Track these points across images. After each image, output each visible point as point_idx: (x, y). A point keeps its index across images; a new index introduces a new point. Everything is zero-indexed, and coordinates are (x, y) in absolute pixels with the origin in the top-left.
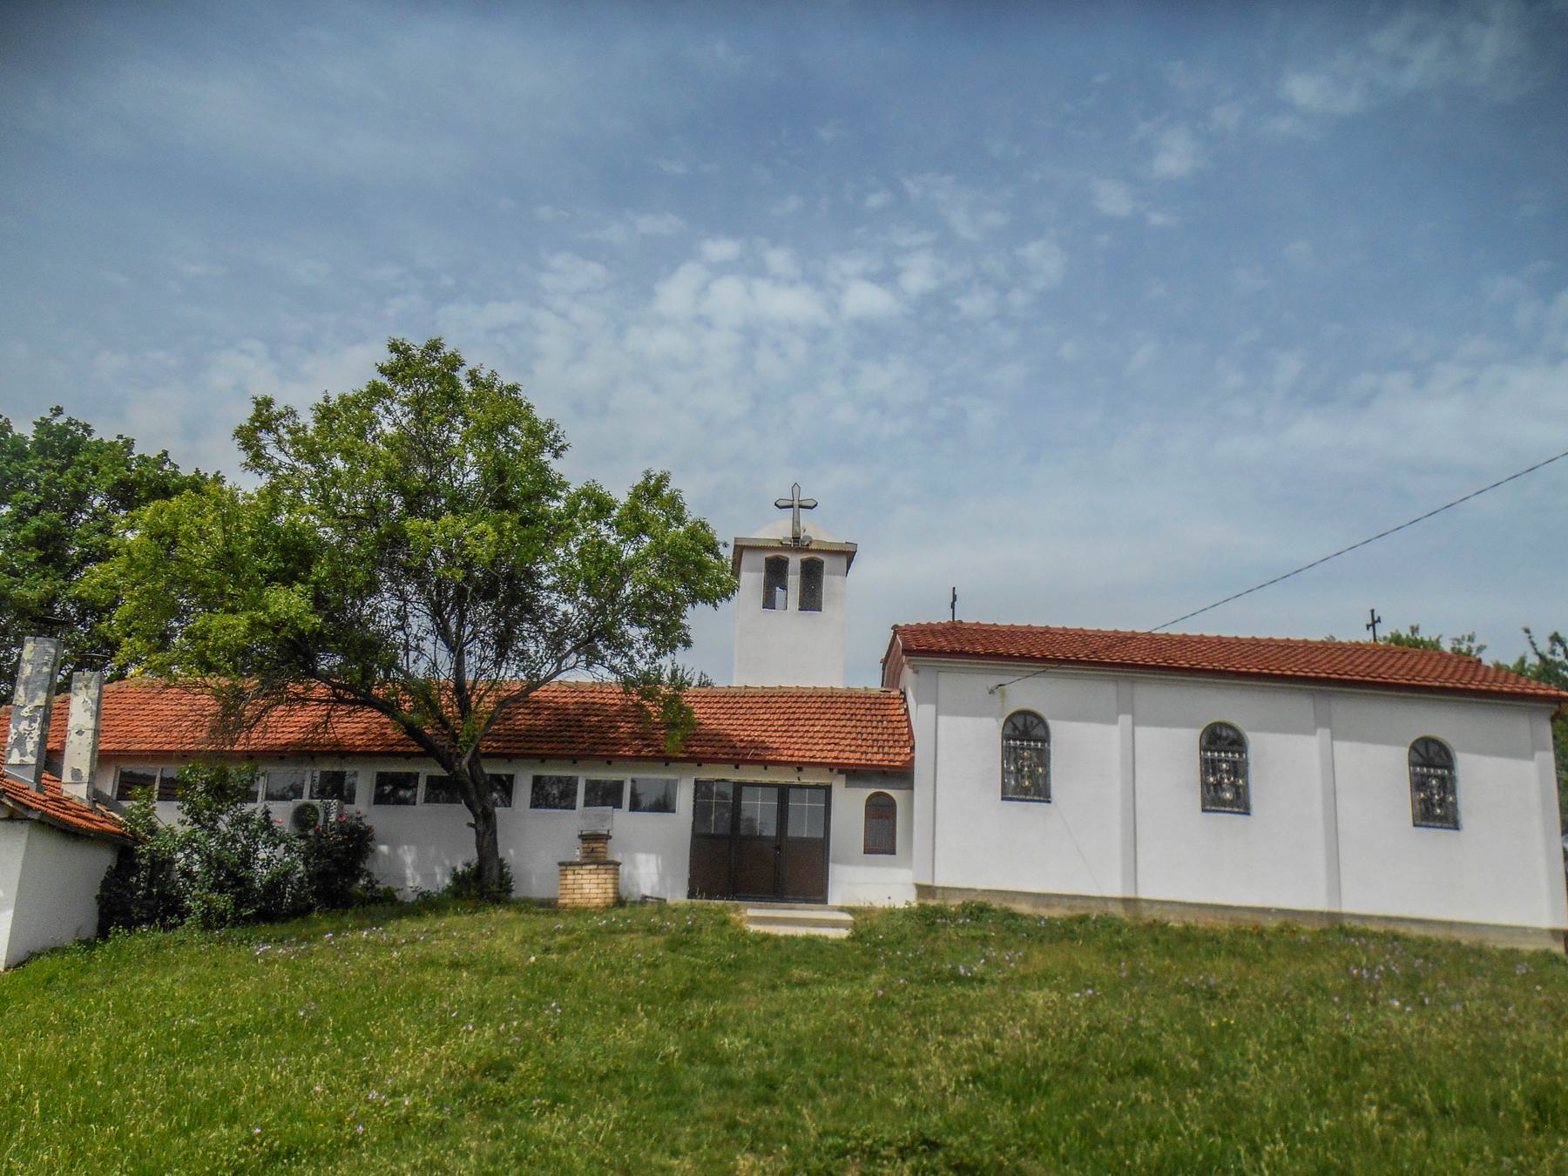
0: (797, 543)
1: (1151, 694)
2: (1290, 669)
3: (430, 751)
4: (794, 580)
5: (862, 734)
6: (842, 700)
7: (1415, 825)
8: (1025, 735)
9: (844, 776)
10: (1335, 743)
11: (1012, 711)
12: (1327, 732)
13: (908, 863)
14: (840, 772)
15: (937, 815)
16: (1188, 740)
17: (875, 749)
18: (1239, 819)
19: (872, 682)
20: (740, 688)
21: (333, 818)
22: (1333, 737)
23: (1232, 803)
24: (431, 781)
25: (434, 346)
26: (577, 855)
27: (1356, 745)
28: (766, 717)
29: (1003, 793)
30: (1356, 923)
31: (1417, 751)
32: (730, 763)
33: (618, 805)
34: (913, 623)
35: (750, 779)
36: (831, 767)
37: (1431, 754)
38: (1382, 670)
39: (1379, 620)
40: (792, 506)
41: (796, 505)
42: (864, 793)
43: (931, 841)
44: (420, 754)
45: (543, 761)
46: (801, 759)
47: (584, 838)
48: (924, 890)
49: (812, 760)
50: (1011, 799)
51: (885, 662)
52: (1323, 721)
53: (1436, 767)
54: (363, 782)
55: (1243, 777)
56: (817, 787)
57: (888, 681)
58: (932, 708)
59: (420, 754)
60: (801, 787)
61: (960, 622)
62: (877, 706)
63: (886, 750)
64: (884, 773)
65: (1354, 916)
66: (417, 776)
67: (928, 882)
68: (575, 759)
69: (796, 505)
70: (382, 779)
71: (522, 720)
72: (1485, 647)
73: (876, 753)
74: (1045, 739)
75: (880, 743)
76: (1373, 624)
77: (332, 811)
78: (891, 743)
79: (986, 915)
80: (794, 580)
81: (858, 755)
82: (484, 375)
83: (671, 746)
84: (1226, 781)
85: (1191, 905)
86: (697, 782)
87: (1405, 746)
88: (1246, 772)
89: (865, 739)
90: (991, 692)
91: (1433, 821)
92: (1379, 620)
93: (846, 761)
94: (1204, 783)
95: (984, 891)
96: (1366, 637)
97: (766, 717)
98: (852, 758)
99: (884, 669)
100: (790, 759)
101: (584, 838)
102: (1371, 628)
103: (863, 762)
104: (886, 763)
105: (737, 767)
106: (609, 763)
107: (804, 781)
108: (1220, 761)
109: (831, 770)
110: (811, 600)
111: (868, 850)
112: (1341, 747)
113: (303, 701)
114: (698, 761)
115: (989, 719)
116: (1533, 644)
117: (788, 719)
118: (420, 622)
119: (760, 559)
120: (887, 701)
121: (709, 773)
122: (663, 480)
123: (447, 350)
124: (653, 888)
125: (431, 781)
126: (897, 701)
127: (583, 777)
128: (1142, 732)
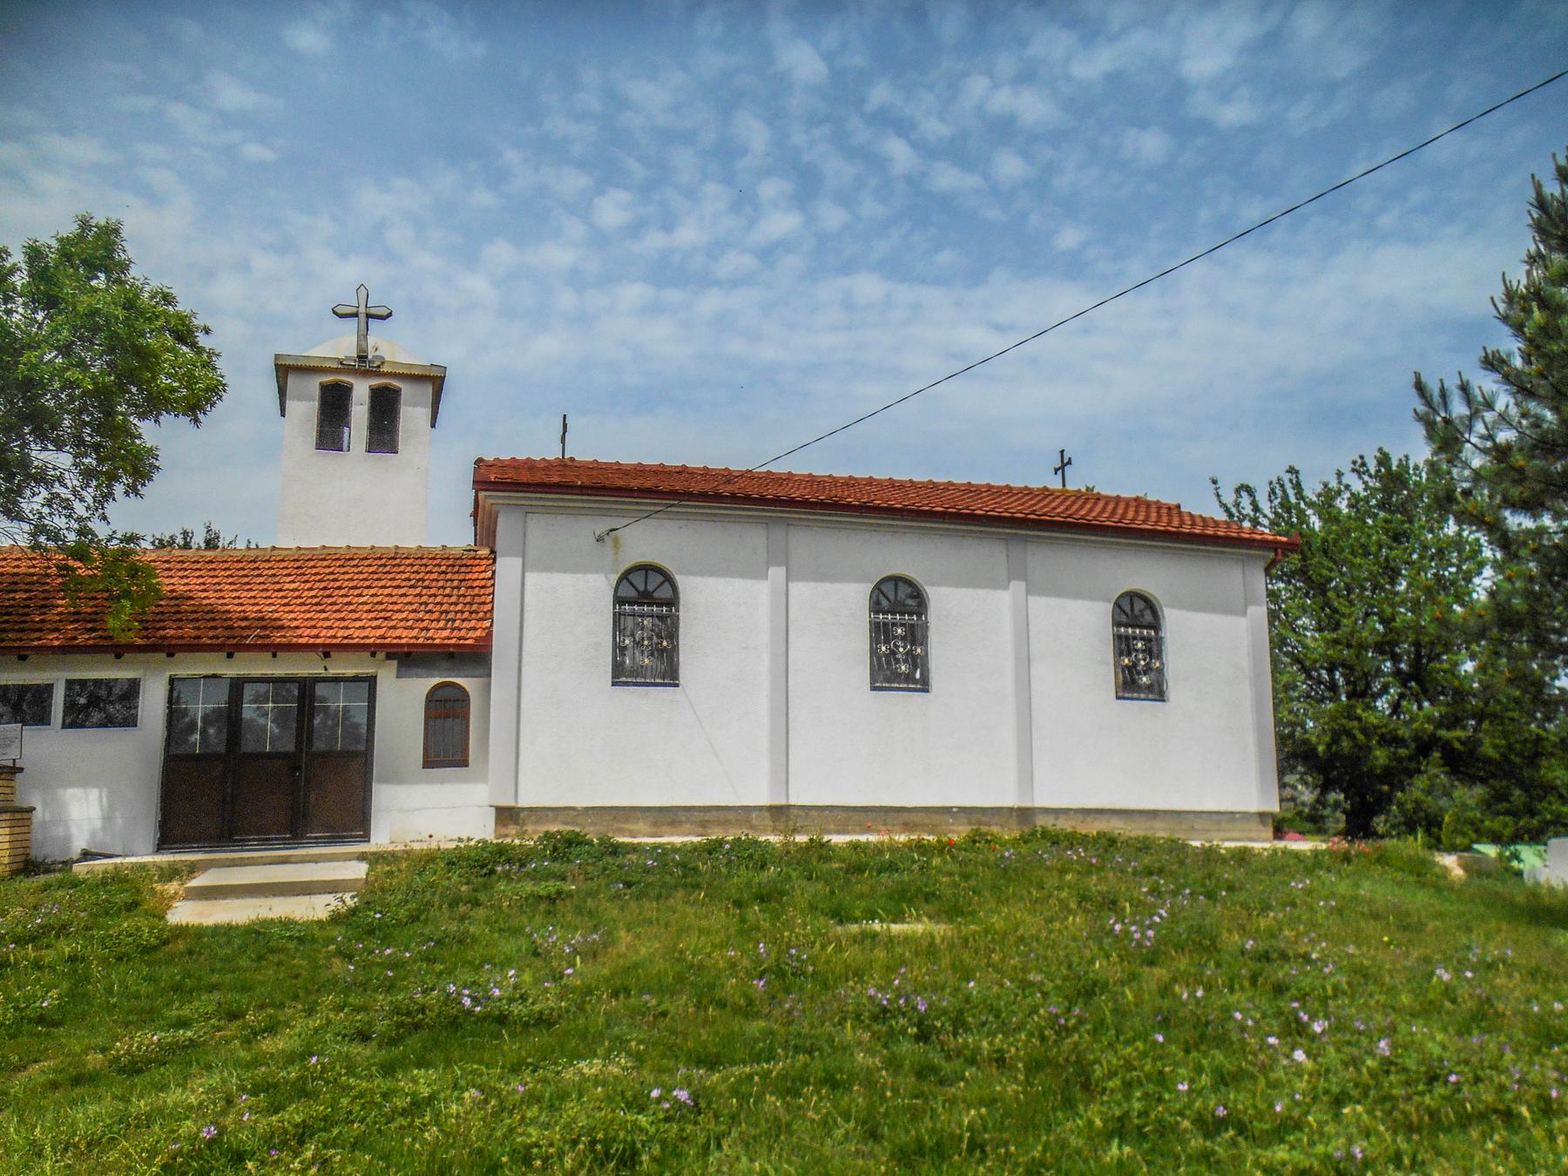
0: (364, 364)
1: (810, 541)
2: (980, 509)
4: (360, 411)
5: (427, 604)
6: (408, 562)
7: (1118, 698)
8: (645, 598)
9: (395, 663)
10: (1030, 598)
11: (627, 566)
12: (1023, 584)
13: (482, 777)
14: (389, 657)
15: (522, 711)
16: (853, 600)
17: (442, 624)
18: (862, 672)
19: (460, 536)
20: (265, 549)
22: (1028, 592)
23: (909, 678)
27: (1053, 601)
28: (293, 586)
30: (1065, 825)
31: (1120, 607)
32: (160, 651)
33: (42, 719)
34: (506, 457)
35: (257, 672)
36: (373, 650)
37: (1136, 612)
38: (1083, 513)
39: (1069, 462)
40: (356, 315)
42: (422, 685)
43: (514, 749)
45: (118, 656)
46: (328, 641)
48: (506, 815)
49: (345, 641)
50: (626, 684)
51: (475, 515)
52: (1018, 572)
53: (1141, 627)
55: (921, 644)
56: (356, 679)
57: (482, 540)
58: (518, 561)
60: (336, 680)
61: (572, 459)
62: (456, 568)
63: (457, 624)
64: (451, 656)
65: (1047, 811)
67: (509, 803)
72: (1418, 375)
73: (442, 629)
75: (451, 616)
76: (1064, 465)
78: (466, 615)
79: (575, 850)
80: (360, 411)
81: (415, 633)
83: (120, 621)
84: (901, 649)
85: (855, 809)
86: (172, 681)
87: (1109, 601)
88: (925, 637)
89: (430, 611)
90: (600, 539)
91: (1138, 692)
92: (1069, 462)
93: (395, 641)
94: (874, 652)
95: (587, 809)
96: (1055, 484)
97: (293, 586)
98: (406, 636)
99: (475, 525)
100: (312, 641)
102: (1060, 472)
103: (421, 641)
104: (453, 641)
105: (274, 655)
106: (23, 658)
107: (333, 671)
108: (894, 624)
109: (373, 654)
110: (383, 435)
111: (428, 764)
112: (1038, 604)
114: (171, 650)
115: (596, 576)
116: (1218, 496)
117: (325, 588)
119: (314, 385)
120: (470, 562)
121: (191, 667)
124: (93, 834)
126: (484, 562)
128: (799, 589)
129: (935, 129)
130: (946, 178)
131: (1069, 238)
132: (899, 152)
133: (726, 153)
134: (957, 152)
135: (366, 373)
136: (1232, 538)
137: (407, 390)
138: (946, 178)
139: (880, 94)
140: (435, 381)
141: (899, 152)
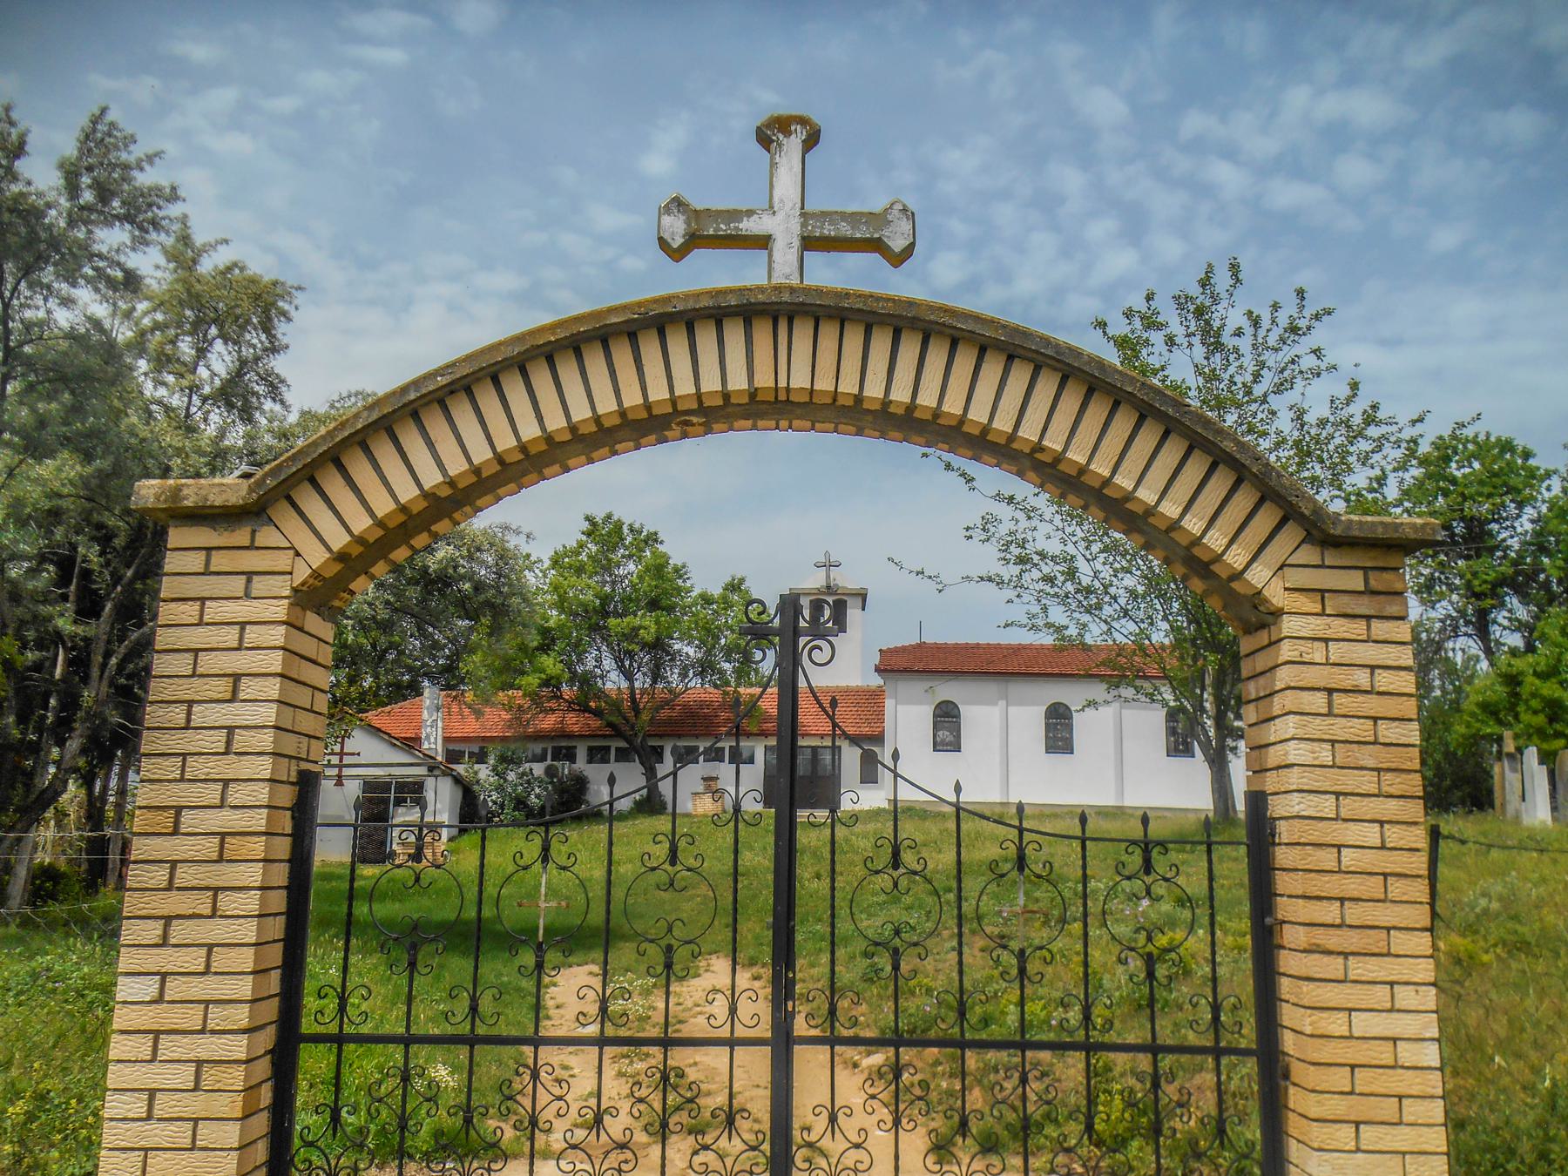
1: (1018, 688)
3: (618, 733)
8: (947, 715)
21: (566, 772)
24: (617, 749)
25: (609, 516)
26: (701, 789)
29: (935, 744)
41: (829, 565)
44: (610, 736)
47: (704, 779)
54: (582, 754)
59: (610, 736)
66: (609, 747)
68: (697, 736)
69: (829, 565)
70: (591, 750)
71: (665, 714)
74: (958, 716)
77: (565, 768)
82: (637, 526)
101: (704, 779)
113: (553, 711)
118: (608, 663)
122: (742, 581)
123: (615, 518)
125: (617, 749)
127: (702, 745)
129: (1264, 146)
130: (1286, 194)
131: (1446, 239)
132: (1226, 175)
133: (1047, 203)
134: (1290, 165)
135: (830, 594)
136: (293, 875)
137: (850, 601)
138: (1286, 194)
139: (1195, 122)
140: (862, 596)
141: (1226, 175)
